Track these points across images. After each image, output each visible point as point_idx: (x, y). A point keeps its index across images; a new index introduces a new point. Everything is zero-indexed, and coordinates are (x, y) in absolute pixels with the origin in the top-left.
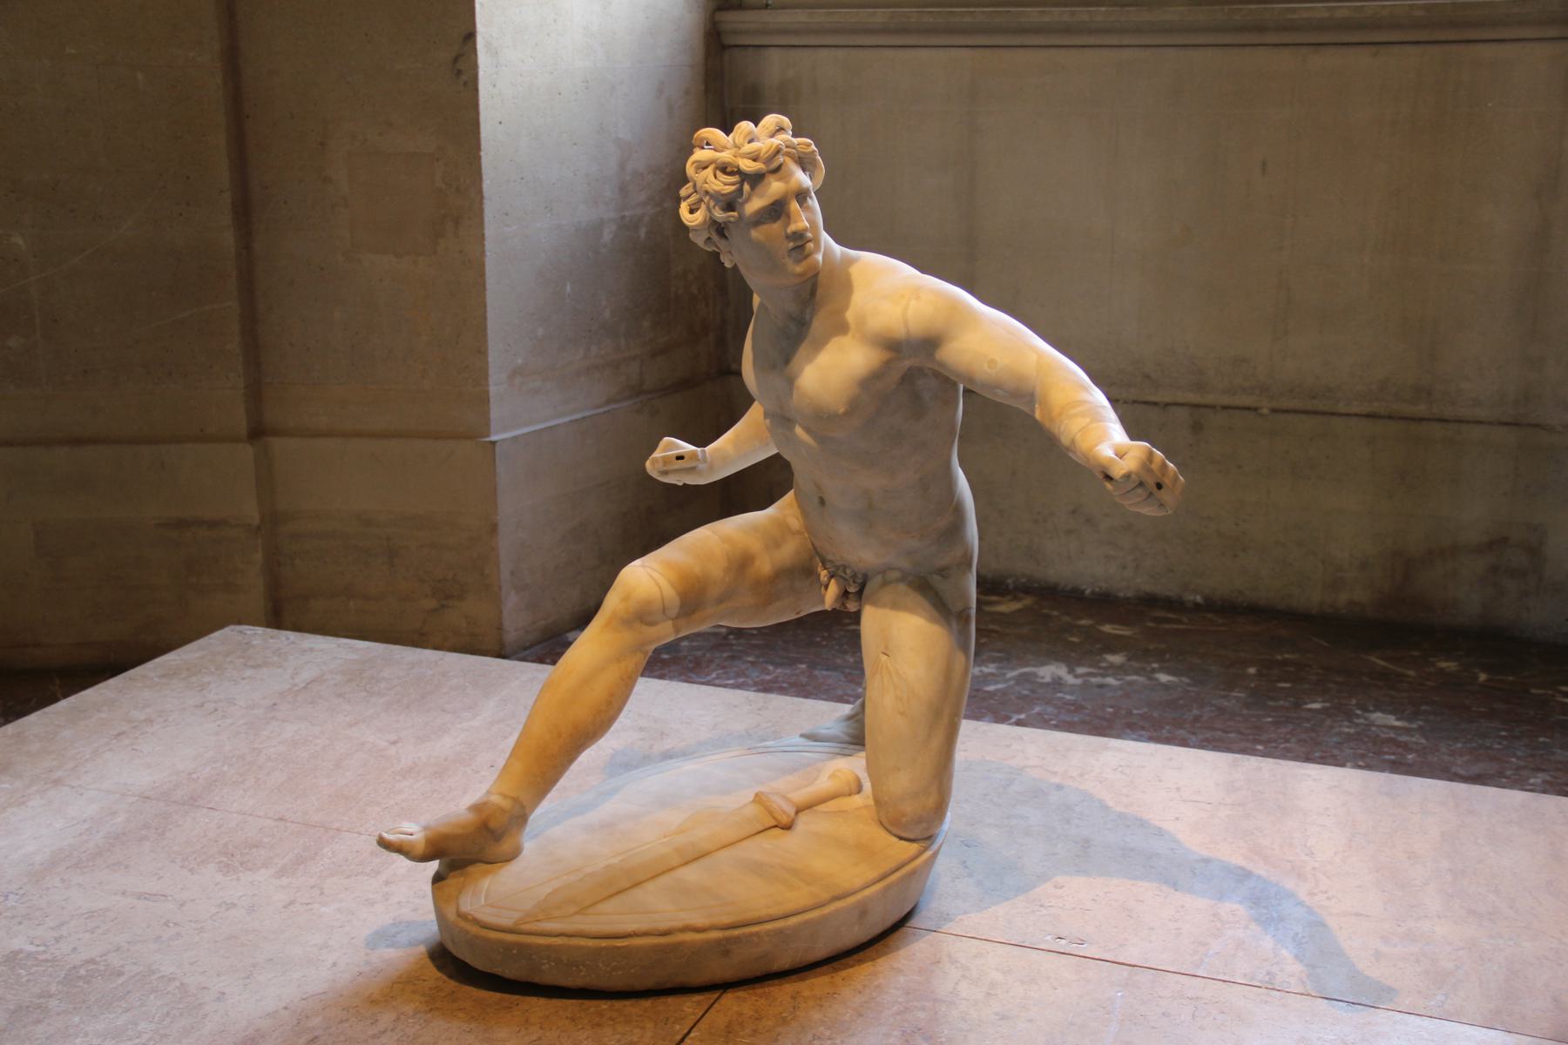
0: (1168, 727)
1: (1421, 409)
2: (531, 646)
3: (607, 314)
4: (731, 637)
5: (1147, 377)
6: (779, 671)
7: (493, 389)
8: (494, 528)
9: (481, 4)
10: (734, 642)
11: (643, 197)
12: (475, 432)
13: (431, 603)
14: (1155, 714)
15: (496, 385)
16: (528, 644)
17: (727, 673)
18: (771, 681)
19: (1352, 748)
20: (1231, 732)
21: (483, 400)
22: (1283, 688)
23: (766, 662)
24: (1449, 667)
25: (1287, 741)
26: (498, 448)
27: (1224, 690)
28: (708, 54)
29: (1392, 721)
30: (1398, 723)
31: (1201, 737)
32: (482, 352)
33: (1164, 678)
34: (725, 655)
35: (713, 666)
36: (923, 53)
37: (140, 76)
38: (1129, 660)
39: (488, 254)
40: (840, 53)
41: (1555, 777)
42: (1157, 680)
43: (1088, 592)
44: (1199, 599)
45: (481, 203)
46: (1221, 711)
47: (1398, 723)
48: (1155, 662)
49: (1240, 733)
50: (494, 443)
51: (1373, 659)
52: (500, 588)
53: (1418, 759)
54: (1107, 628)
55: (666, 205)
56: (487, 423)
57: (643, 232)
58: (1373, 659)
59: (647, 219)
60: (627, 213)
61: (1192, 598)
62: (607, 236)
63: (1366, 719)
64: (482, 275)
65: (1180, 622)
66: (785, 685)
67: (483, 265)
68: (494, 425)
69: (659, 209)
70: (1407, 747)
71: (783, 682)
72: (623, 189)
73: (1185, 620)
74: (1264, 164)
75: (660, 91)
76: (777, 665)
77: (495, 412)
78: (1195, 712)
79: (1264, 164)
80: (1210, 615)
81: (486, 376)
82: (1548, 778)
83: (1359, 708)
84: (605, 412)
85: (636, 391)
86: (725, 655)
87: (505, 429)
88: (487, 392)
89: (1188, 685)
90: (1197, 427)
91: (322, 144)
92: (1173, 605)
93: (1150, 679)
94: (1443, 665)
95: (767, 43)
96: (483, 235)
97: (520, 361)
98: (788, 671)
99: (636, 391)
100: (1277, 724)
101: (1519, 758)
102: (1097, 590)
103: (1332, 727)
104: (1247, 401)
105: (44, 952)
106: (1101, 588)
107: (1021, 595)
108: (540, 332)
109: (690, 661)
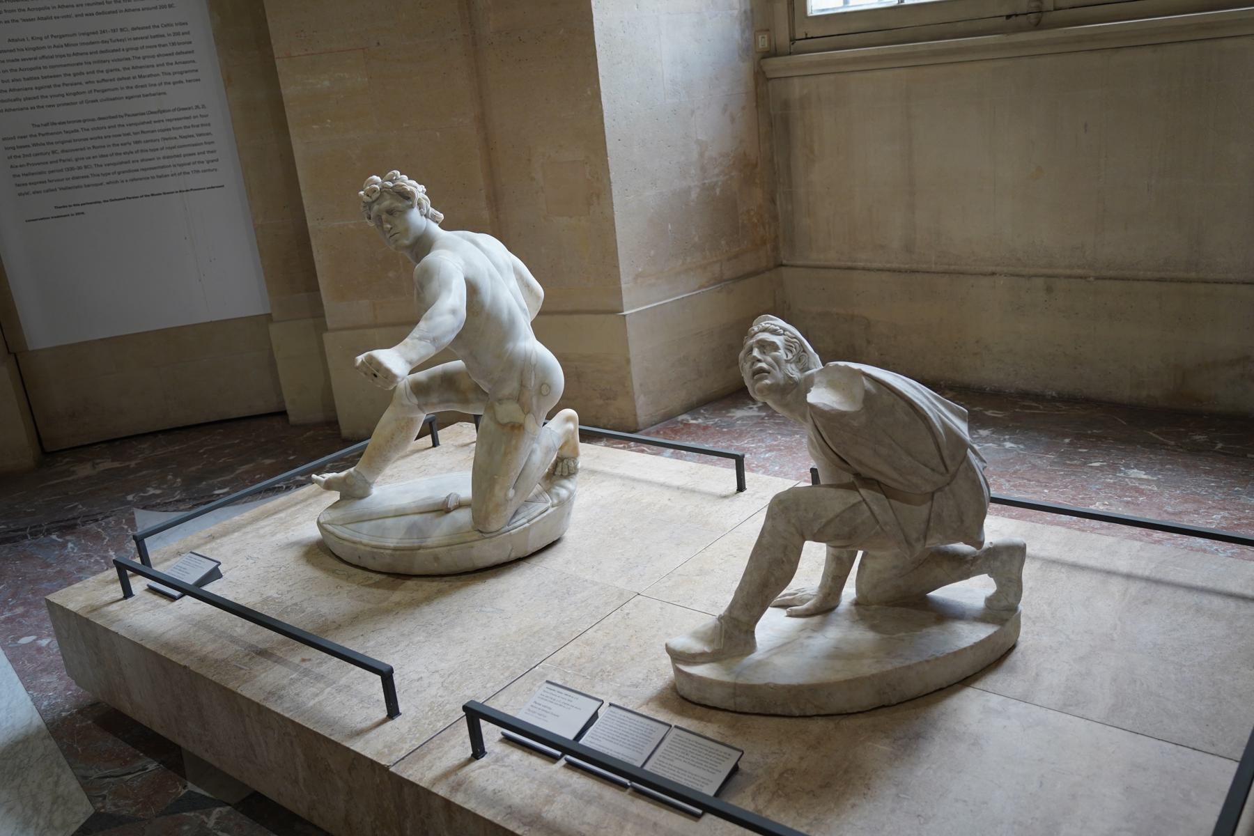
0: (994, 477)
1: (1193, 275)
2: (655, 424)
3: (696, 239)
4: (766, 418)
5: (1019, 260)
6: (783, 439)
7: (623, 286)
8: (628, 361)
9: (603, 76)
10: (766, 421)
11: (716, 171)
12: (616, 311)
13: (600, 402)
14: (10, 626)
15: (625, 283)
16: (654, 423)
17: (753, 440)
18: (776, 445)
19: (1106, 493)
20: (1032, 481)
21: (619, 292)
22: (1081, 452)
23: (778, 434)
24: (1200, 439)
25: (1066, 487)
26: (627, 318)
27: (1042, 453)
28: (757, 85)
29: (1142, 475)
30: (1145, 477)
31: (1012, 483)
32: (617, 267)
33: (1008, 445)
34: (758, 429)
35: (749, 435)
36: (879, 73)
37: (438, 134)
38: (993, 433)
39: (616, 212)
40: (832, 77)
41: (1232, 515)
42: (1003, 446)
43: (988, 389)
44: (1054, 394)
45: (610, 186)
46: (1034, 466)
47: (1145, 477)
48: (1007, 435)
49: (1038, 481)
50: (625, 316)
51: (1151, 433)
52: (634, 394)
53: (1146, 501)
54: (989, 413)
55: (733, 174)
56: (622, 305)
57: (718, 191)
58: (1151, 433)
59: (720, 183)
60: (706, 181)
61: (1050, 393)
62: (694, 195)
63: (1125, 473)
64: (613, 225)
65: (1037, 408)
66: (782, 448)
67: (613, 219)
68: (625, 308)
69: (727, 177)
70: (1141, 492)
71: (782, 446)
72: (703, 169)
73: (1041, 407)
74: (1086, 125)
75: (725, 110)
76: (783, 435)
77: (626, 299)
78: (1017, 467)
79: (1086, 125)
80: (1058, 404)
81: (619, 279)
82: (1227, 515)
83: (1124, 467)
84: (696, 294)
85: (719, 280)
86: (758, 429)
87: (633, 308)
88: (621, 288)
89: (1022, 450)
90: (1049, 290)
91: (529, 160)
92: (1039, 398)
93: (999, 445)
94: (1197, 437)
95: (791, 75)
96: (612, 203)
97: (640, 270)
98: (788, 439)
99: (719, 280)
100: (1064, 476)
101: (1214, 501)
102: (993, 388)
103: (1100, 478)
104: (1080, 272)
105: (280, 598)
106: (995, 387)
107: (947, 391)
108: (652, 253)
109: (737, 433)
